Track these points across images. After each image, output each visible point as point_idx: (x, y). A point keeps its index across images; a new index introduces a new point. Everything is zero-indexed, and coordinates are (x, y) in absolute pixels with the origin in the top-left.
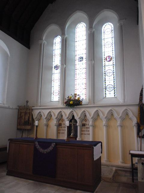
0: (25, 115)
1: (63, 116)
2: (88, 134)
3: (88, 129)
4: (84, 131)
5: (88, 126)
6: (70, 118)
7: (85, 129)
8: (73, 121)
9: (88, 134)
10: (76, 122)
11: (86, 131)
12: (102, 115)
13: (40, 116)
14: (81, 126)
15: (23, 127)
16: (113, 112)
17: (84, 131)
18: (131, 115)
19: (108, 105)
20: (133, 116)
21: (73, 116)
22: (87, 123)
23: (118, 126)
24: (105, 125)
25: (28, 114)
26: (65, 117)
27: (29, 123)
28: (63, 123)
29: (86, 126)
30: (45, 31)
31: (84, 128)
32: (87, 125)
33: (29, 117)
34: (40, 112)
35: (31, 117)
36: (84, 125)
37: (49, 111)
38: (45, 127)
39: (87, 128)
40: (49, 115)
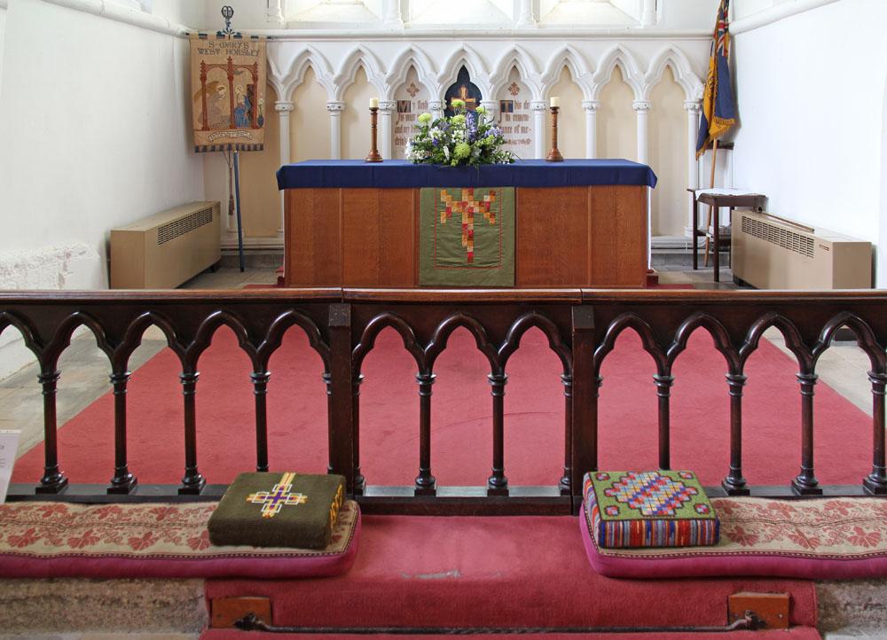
0: (231, 78)
1: (367, 69)
2: (523, 142)
3: (523, 124)
4: (509, 129)
5: (522, 111)
6: (399, 80)
7: (513, 124)
8: (464, 90)
9: (523, 142)
10: (474, 92)
11: (517, 128)
12: (429, 70)
13: (307, 66)
14: (495, 110)
15: (233, 134)
16: (570, 59)
17: (509, 129)
18: (684, 70)
19: (466, 33)
20: (692, 74)
21: (464, 73)
22: (520, 98)
23: (585, 109)
24: (594, 106)
25: (248, 75)
26: (425, 73)
27: (251, 114)
28: (413, 100)
29: (516, 111)
30: (231, 298)
31: (508, 118)
32: (519, 105)
33: (251, 91)
34: (307, 52)
35: (261, 86)
36: (505, 107)
37: (353, 47)
38: (333, 120)
39: (519, 118)
40: (304, 61)
